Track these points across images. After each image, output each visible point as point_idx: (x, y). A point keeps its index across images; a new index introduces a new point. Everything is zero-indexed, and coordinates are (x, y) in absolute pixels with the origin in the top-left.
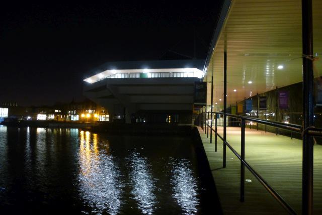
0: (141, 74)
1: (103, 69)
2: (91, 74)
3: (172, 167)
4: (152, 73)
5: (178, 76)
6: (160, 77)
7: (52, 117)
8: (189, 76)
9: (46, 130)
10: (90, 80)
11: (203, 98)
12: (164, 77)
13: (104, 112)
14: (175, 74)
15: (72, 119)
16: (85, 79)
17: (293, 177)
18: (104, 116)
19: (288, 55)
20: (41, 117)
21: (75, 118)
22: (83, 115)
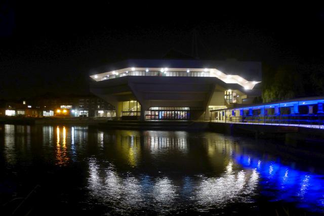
0: (110, 76)
1: (121, 66)
2: (101, 71)
3: (97, 136)
4: (173, 72)
5: (195, 76)
6: (178, 76)
7: (22, 113)
8: (205, 76)
9: (16, 112)
10: (96, 77)
11: (264, 102)
12: (181, 76)
13: (83, 107)
14: (192, 73)
15: (44, 115)
16: (91, 75)
17: (130, 122)
18: (82, 111)
19: (129, 72)
20: (10, 113)
21: (51, 113)
22: (58, 111)
